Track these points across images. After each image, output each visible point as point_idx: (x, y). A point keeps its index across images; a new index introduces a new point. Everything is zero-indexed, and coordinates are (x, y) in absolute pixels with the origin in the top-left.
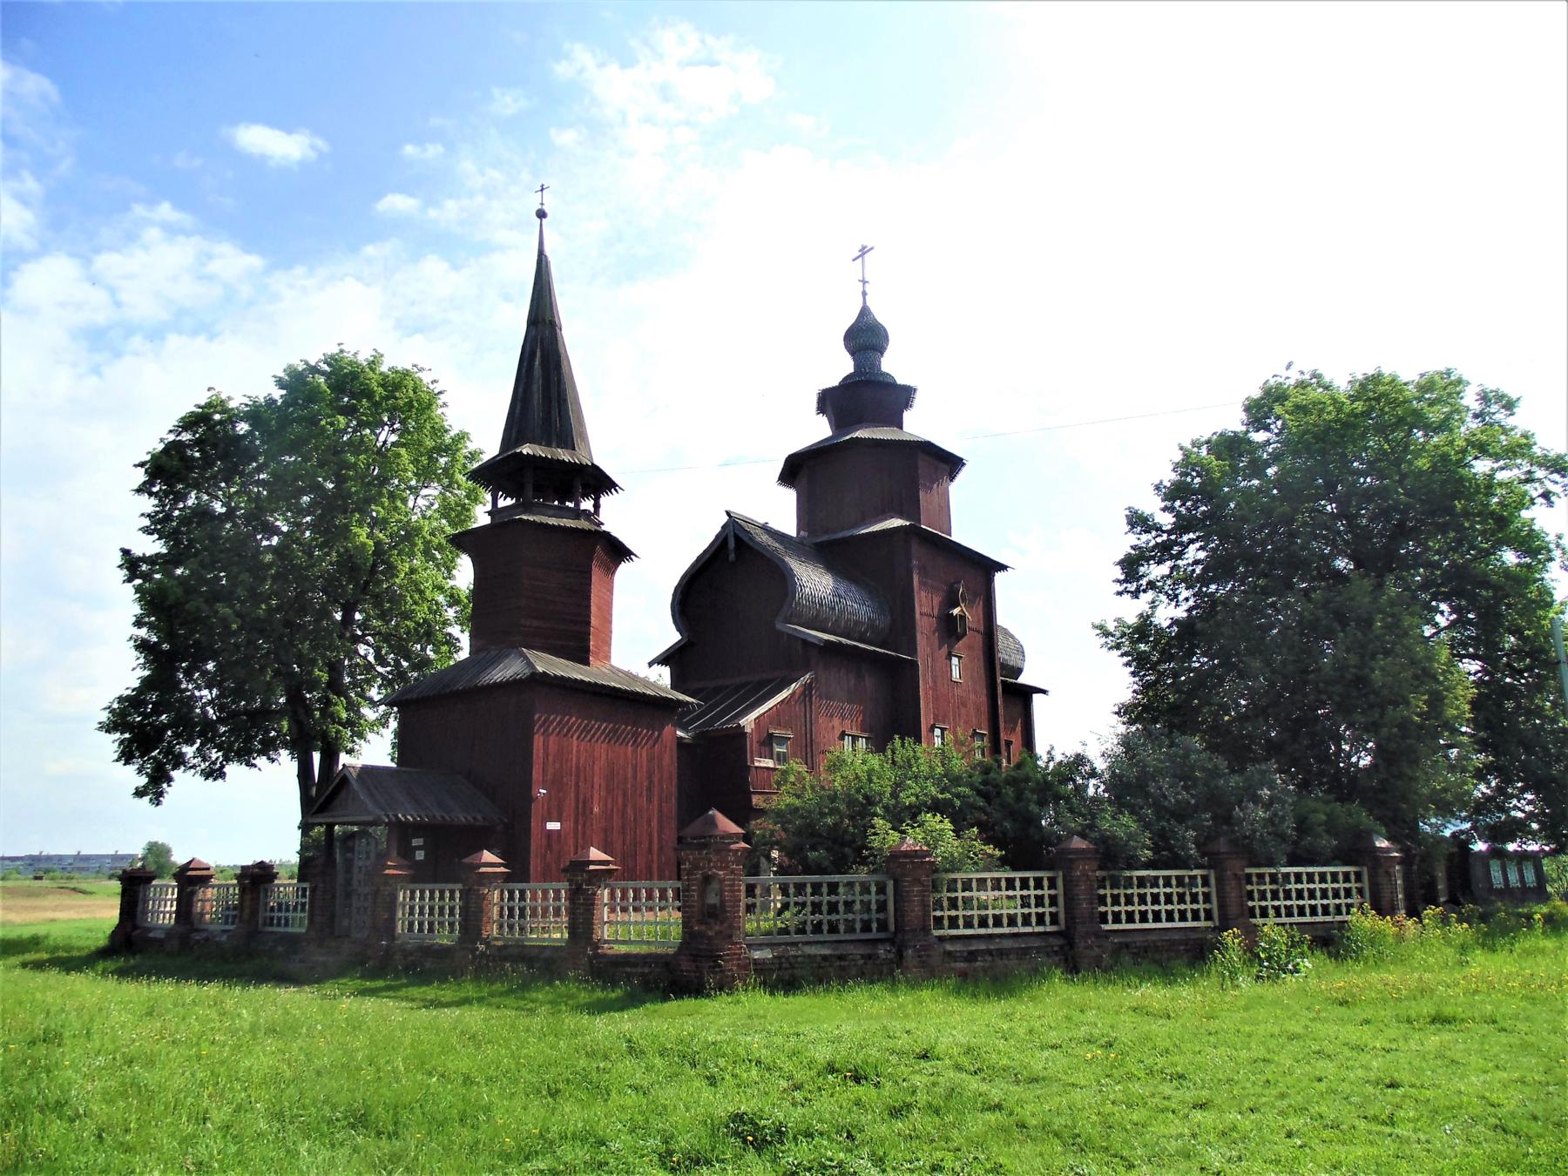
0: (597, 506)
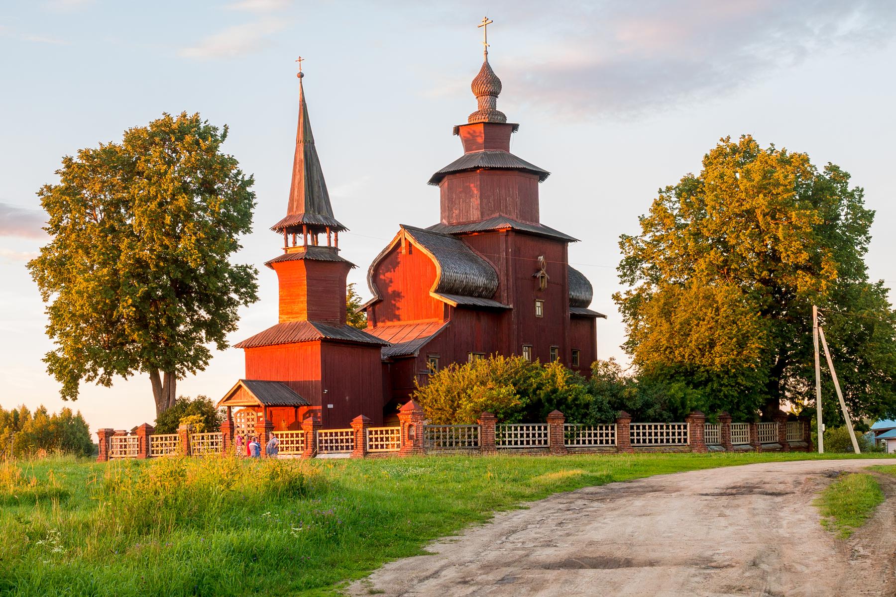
0: (336, 240)
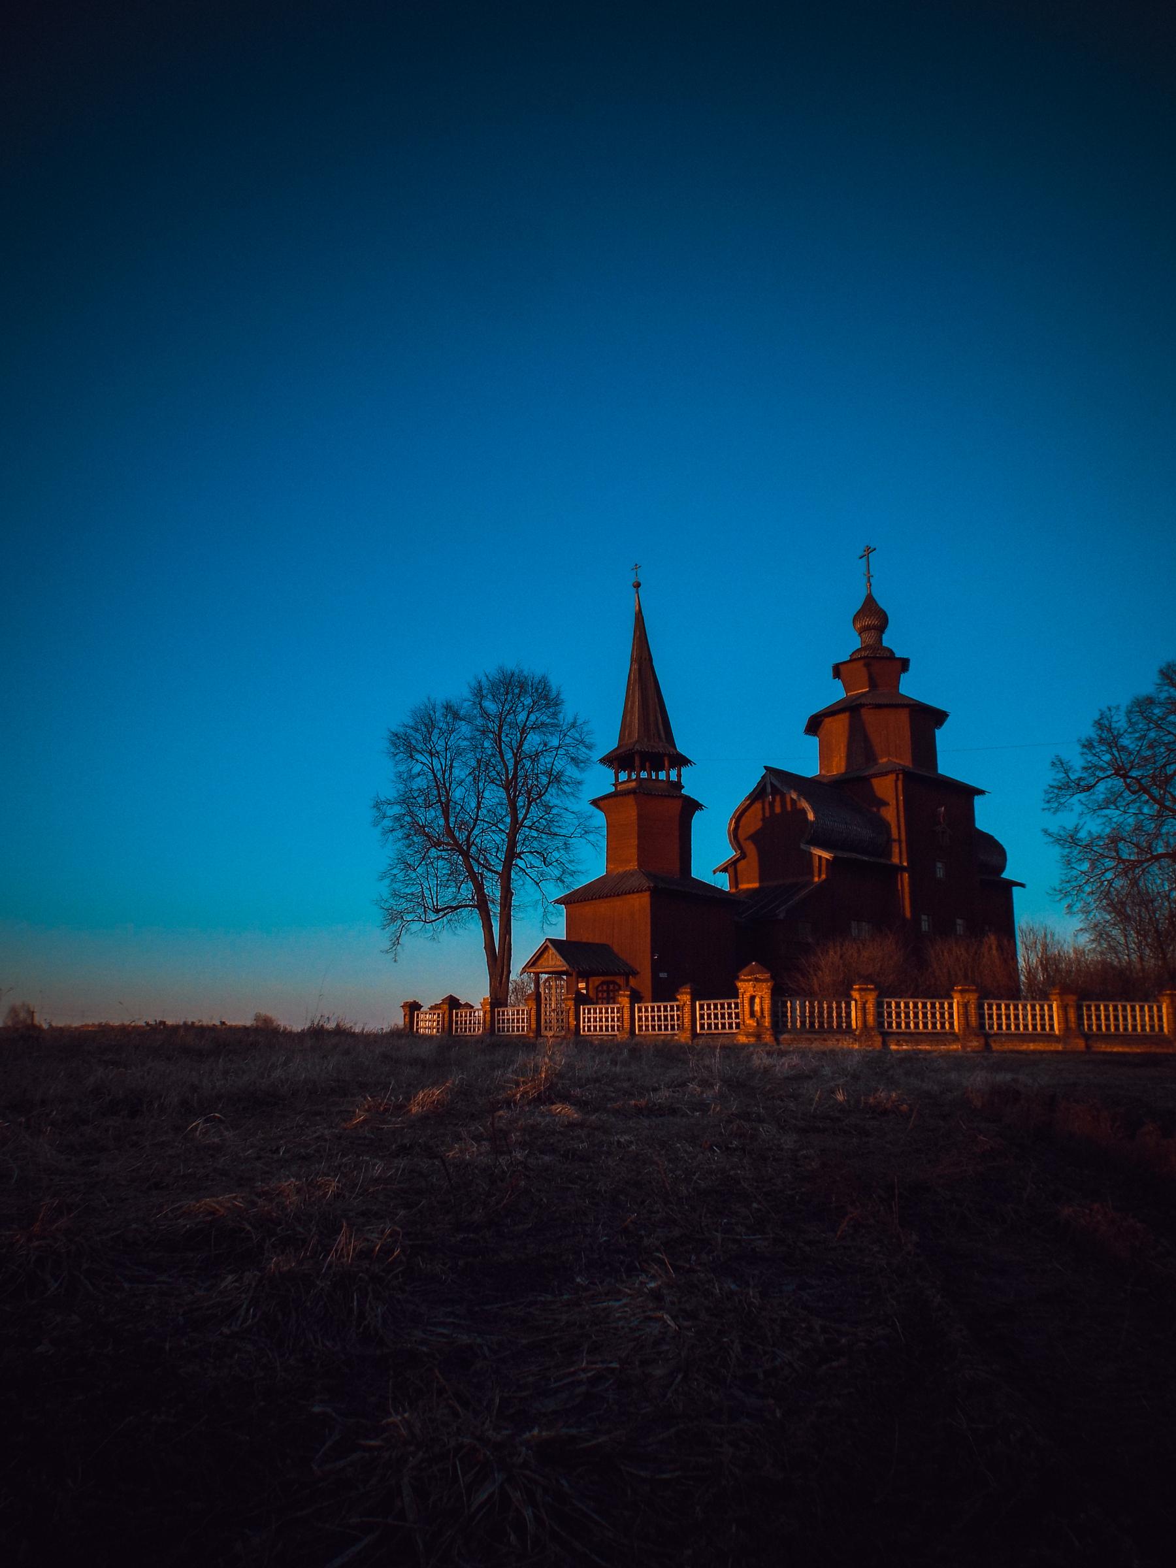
0: (679, 776)
